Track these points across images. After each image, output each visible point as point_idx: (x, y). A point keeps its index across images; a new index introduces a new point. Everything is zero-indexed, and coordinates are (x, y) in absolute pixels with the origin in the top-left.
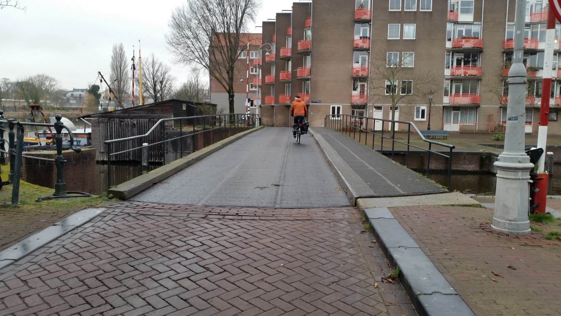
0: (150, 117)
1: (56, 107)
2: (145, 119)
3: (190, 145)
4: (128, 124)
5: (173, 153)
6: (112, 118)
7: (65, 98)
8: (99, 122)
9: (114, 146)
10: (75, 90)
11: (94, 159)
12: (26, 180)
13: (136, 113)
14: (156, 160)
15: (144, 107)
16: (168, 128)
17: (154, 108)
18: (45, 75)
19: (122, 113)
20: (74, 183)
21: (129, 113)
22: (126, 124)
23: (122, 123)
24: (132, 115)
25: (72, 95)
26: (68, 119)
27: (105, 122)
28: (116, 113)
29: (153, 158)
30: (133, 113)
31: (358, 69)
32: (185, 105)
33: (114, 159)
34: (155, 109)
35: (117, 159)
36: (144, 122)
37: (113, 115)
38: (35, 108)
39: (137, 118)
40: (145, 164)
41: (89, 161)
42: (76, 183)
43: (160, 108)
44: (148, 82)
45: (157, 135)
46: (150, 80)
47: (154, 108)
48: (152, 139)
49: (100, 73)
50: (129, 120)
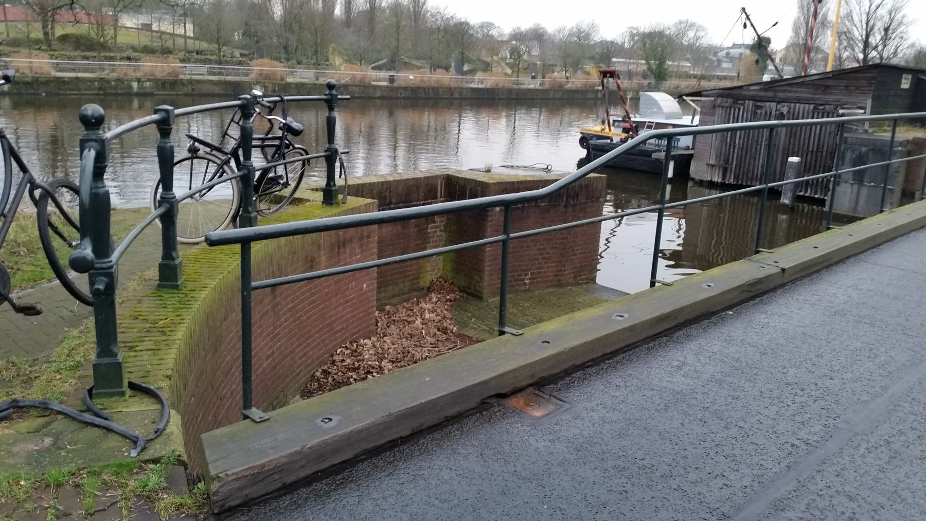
0: (817, 102)
1: (693, 74)
2: (807, 105)
3: (897, 172)
4: (771, 113)
5: (852, 184)
6: (740, 100)
7: (714, 59)
8: (714, 107)
9: (735, 156)
10: (735, 46)
11: (598, 198)
12: (442, 228)
13: (790, 92)
14: (816, 193)
15: (808, 79)
16: (855, 127)
17: (831, 83)
18: (689, 21)
19: (760, 90)
20: (539, 250)
21: (776, 91)
22: (766, 113)
23: (759, 111)
24: (781, 95)
25: (728, 54)
26: (671, 95)
27: (727, 107)
28: (751, 90)
29: (809, 189)
30: (784, 91)
31: (828, 204)
32: (910, 77)
33: (732, 181)
34: (831, 84)
35: (738, 181)
36: (803, 111)
37: (744, 93)
38: (608, 75)
39: (791, 103)
40: (787, 201)
41: (585, 203)
42: (545, 249)
43: (844, 83)
44: (855, 29)
45: (826, 140)
46: (858, 25)
47: (831, 83)
48: (815, 149)
49: (744, 9)
50: (773, 105)
